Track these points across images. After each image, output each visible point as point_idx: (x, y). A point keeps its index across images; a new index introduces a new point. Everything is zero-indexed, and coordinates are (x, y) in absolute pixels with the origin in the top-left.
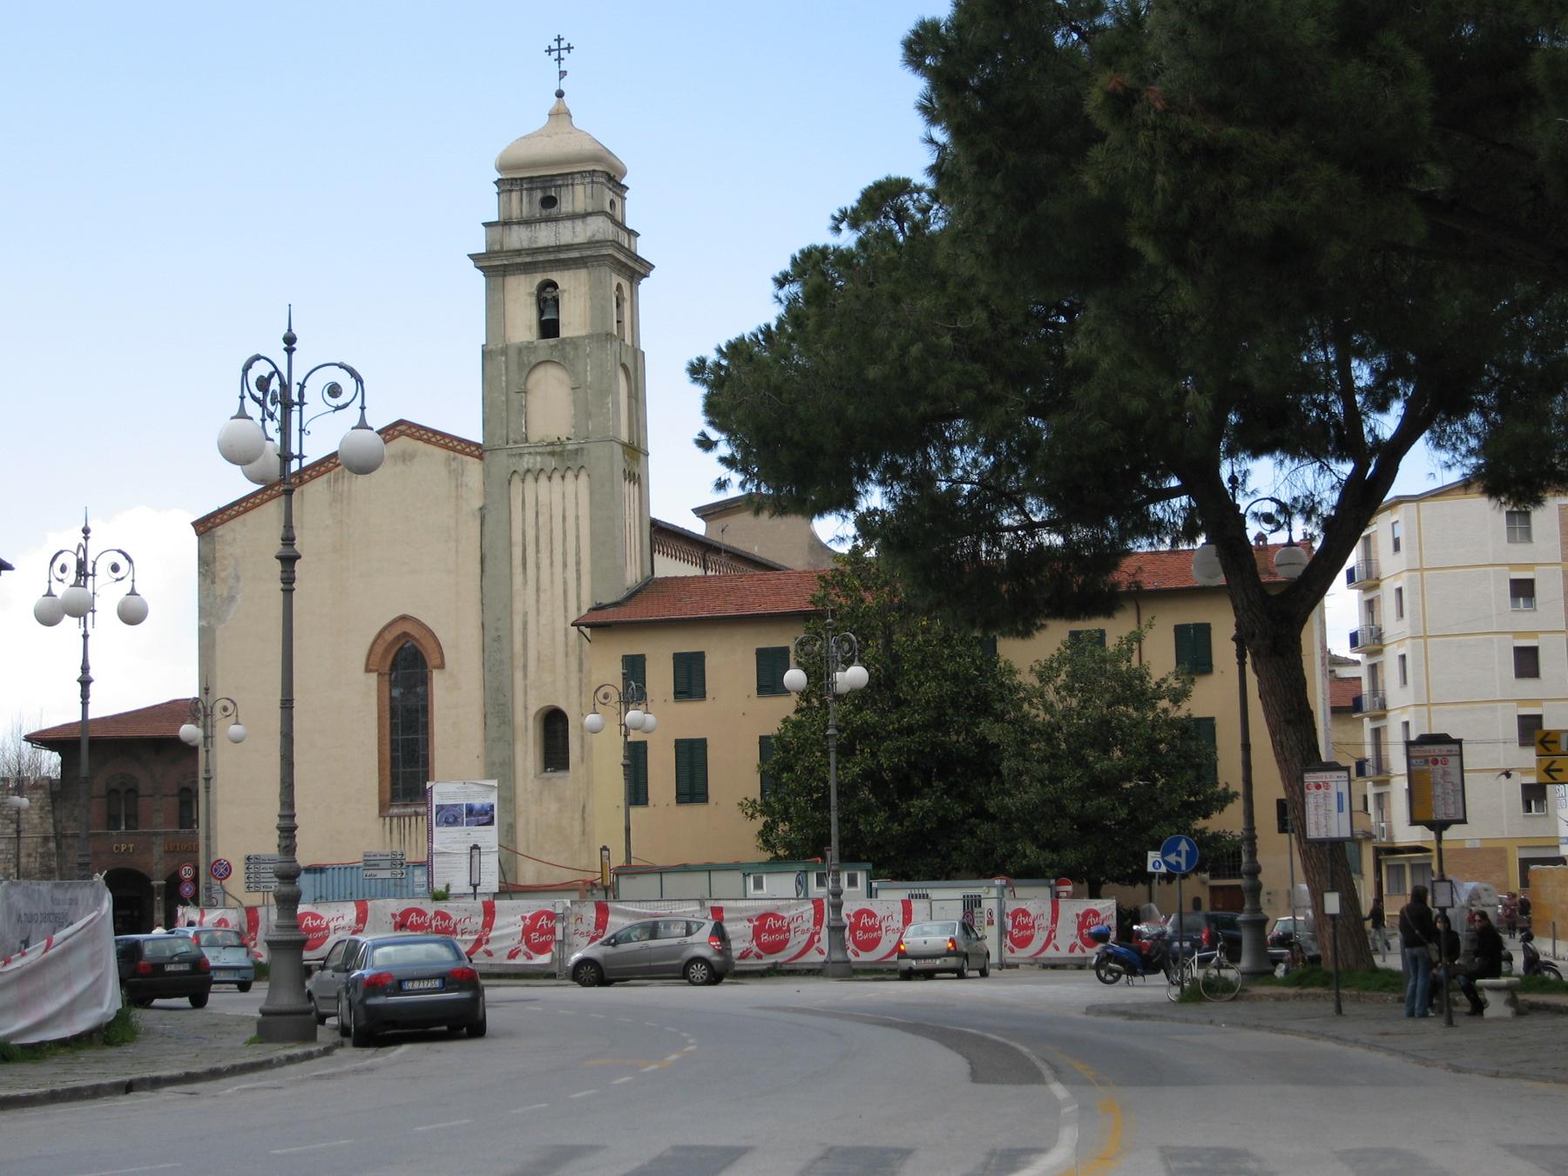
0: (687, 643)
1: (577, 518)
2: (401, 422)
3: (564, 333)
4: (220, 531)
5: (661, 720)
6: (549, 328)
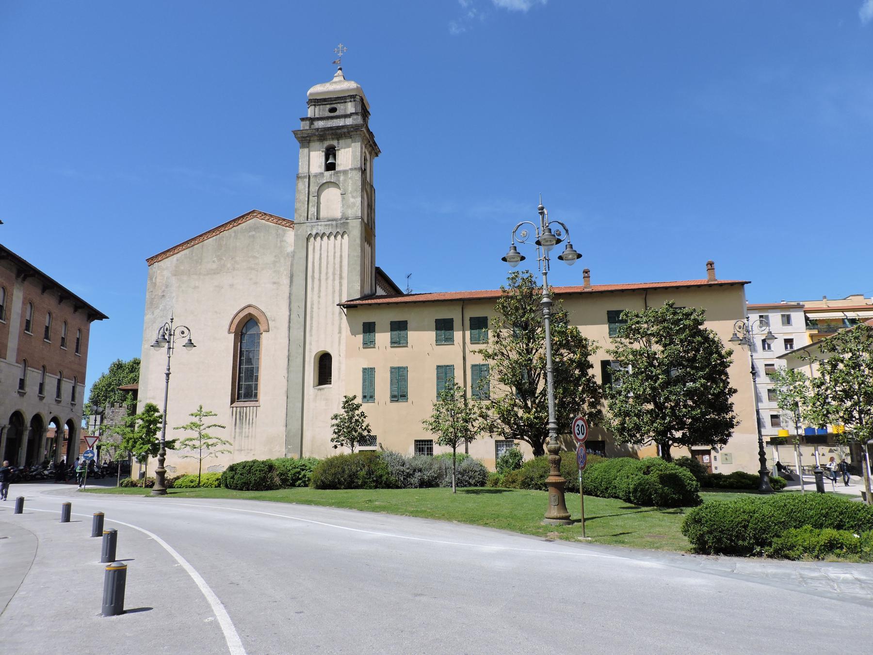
1: (341, 256)
3: (338, 168)
6: (330, 167)
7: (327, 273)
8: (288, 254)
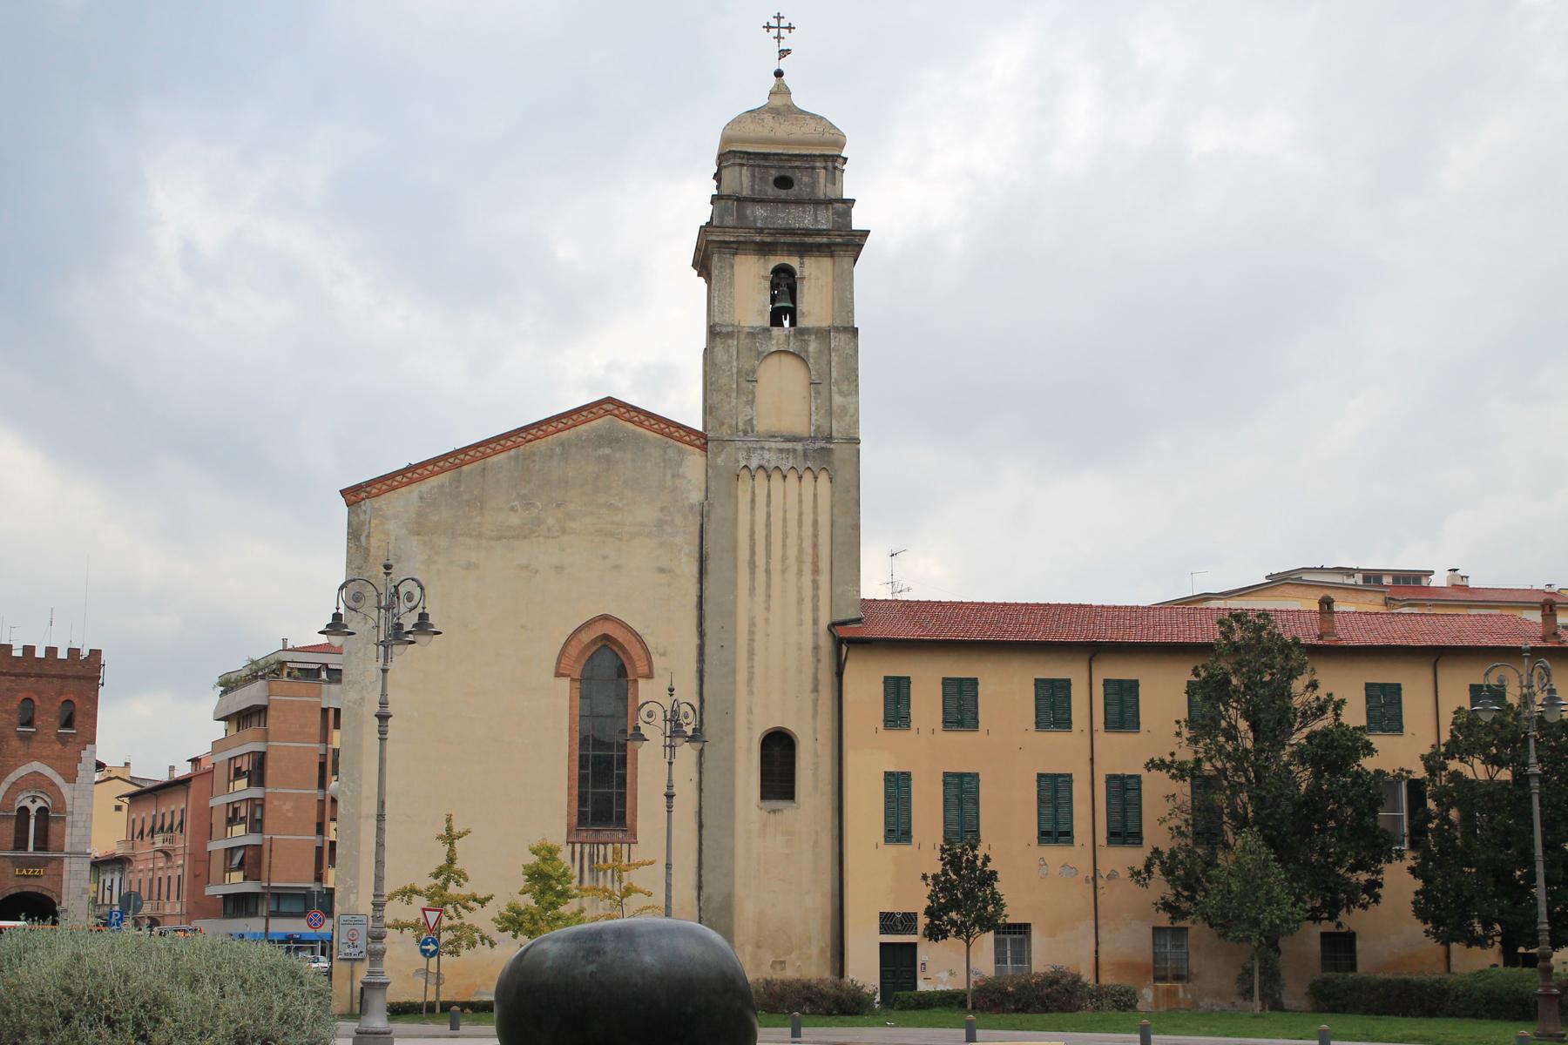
0: (959, 668)
2: (609, 400)
4: (367, 505)
5: (928, 750)
8: (692, 507)
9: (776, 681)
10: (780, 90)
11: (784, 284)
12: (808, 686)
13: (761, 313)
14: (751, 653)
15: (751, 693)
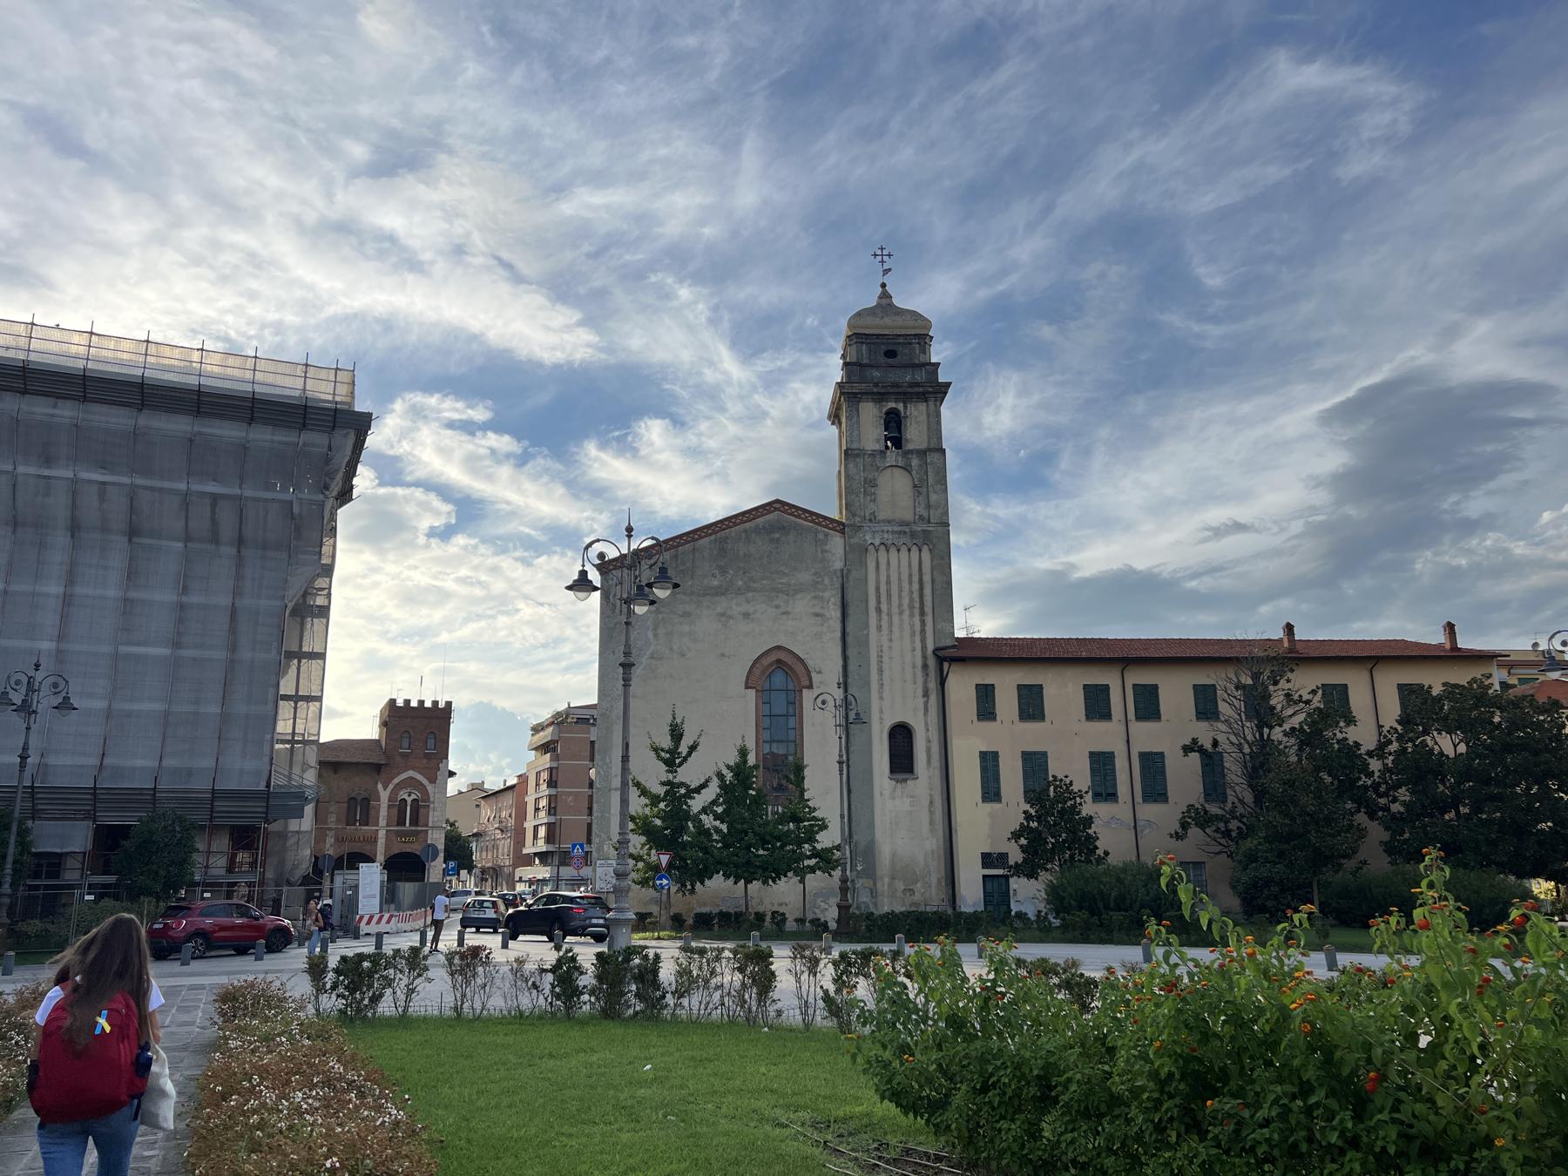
2: (778, 501)
7: (900, 605)
9: (896, 697)
10: (885, 295)
11: (894, 423)
12: (920, 692)
13: (878, 441)
14: (881, 671)
15: (881, 698)
